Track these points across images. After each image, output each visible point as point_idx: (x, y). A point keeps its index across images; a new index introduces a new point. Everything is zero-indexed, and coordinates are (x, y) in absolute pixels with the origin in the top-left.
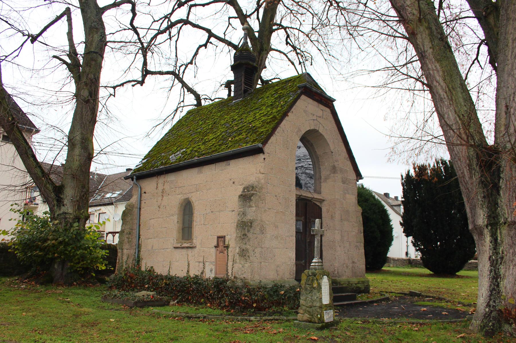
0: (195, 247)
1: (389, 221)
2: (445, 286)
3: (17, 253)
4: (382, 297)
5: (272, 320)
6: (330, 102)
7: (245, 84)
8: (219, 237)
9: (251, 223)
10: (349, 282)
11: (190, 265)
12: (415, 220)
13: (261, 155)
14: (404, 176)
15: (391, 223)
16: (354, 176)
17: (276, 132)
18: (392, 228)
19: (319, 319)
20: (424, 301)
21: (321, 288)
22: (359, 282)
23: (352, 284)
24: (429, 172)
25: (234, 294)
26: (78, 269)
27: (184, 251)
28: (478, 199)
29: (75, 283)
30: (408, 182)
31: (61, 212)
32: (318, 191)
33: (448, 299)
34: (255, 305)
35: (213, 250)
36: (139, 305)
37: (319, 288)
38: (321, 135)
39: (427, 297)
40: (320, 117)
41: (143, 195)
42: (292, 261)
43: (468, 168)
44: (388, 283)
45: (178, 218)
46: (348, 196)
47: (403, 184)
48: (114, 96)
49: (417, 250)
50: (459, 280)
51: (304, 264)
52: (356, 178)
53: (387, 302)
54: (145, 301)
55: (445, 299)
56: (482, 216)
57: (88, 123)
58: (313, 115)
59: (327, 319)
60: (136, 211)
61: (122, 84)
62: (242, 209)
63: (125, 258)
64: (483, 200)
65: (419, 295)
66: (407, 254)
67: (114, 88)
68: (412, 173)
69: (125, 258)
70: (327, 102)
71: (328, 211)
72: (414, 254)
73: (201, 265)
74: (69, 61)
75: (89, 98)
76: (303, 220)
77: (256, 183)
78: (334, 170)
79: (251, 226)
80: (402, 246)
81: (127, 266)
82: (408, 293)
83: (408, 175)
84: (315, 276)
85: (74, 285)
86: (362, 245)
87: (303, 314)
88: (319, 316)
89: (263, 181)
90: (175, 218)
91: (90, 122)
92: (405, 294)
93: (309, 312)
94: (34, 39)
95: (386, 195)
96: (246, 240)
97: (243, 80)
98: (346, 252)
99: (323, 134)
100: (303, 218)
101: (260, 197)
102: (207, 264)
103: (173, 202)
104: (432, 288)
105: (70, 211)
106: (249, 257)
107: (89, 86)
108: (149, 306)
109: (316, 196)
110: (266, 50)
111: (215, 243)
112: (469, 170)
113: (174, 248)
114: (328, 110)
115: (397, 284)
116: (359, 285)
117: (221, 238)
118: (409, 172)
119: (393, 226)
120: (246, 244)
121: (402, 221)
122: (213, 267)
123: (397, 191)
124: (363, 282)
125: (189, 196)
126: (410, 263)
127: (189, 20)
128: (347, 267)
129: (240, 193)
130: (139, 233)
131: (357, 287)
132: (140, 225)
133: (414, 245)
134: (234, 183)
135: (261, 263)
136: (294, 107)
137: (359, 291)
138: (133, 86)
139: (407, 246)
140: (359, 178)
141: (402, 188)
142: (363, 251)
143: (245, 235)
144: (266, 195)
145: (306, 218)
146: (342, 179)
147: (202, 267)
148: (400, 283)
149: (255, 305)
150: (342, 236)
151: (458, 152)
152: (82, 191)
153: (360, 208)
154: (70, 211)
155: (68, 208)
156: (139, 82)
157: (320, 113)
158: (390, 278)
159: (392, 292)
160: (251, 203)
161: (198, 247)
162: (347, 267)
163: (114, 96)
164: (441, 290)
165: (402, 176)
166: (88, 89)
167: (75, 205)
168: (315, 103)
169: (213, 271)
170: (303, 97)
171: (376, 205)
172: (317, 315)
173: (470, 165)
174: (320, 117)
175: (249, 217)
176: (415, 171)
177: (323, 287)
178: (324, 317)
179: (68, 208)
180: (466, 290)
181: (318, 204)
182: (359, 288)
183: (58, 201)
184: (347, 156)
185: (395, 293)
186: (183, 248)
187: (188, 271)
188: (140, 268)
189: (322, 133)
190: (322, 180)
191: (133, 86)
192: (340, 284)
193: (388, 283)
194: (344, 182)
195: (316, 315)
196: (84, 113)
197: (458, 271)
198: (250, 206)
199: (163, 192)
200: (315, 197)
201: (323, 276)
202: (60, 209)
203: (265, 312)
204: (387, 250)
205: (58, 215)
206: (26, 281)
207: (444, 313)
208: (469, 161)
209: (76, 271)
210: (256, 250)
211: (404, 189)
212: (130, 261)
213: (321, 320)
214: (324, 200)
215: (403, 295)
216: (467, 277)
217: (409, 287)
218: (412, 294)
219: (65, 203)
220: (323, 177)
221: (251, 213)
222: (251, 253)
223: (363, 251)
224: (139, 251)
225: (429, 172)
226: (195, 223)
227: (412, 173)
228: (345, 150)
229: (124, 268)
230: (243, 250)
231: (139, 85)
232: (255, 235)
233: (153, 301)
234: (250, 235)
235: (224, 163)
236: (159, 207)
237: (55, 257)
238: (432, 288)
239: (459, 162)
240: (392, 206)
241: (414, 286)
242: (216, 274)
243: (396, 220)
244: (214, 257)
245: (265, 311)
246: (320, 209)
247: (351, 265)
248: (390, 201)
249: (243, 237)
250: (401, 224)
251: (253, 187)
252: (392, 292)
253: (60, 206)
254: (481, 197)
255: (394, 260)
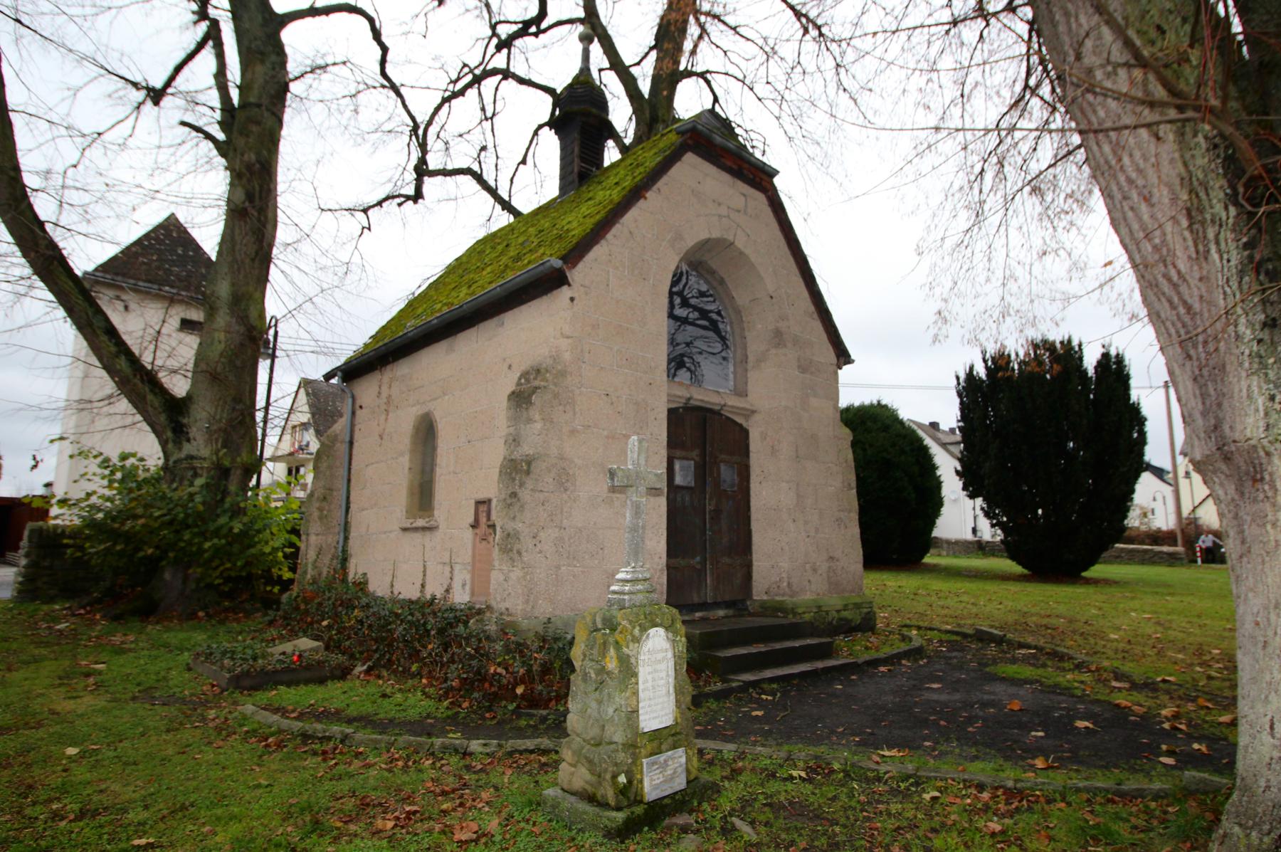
0: (436, 528)
1: (934, 468)
2: (1062, 609)
3: (67, 546)
4: (904, 647)
5: (532, 752)
6: (764, 177)
7: (582, 159)
8: (479, 503)
9: (529, 464)
10: (820, 607)
11: (428, 573)
12: (988, 464)
13: (565, 288)
14: (962, 376)
15: (938, 473)
16: (830, 355)
17: (609, 236)
18: (940, 483)
19: (623, 791)
20: (1014, 661)
21: (635, 675)
22: (846, 605)
23: (827, 612)
24: (1016, 367)
25: (472, 657)
26: (217, 582)
27: (417, 537)
28: (1238, 337)
29: (201, 614)
30: (974, 393)
31: (183, 455)
32: (741, 392)
33: (1081, 657)
34: (520, 690)
35: (469, 534)
36: (247, 682)
37: (628, 671)
38: (741, 253)
39: (1021, 646)
40: (739, 211)
41: (359, 412)
42: (657, 559)
43: (1185, 223)
44: (928, 599)
45: (411, 460)
46: (814, 402)
47: (960, 394)
48: (369, 229)
49: (993, 526)
50: (1091, 590)
51: (698, 567)
52: (834, 360)
53: (916, 660)
54: (267, 673)
55: (1071, 658)
56: (1261, 401)
57: (247, 261)
58: (720, 204)
59: (656, 787)
60: (342, 448)
61: (380, 203)
62: (512, 429)
63: (312, 555)
64: (1265, 335)
65: (999, 641)
66: (974, 531)
67: (365, 211)
68: (980, 371)
69: (312, 555)
70: (758, 177)
71: (764, 437)
72: (988, 532)
73: (448, 569)
74: (221, 136)
75: (247, 204)
76: (697, 459)
77: (549, 361)
78: (778, 338)
79: (528, 473)
80: (961, 516)
81: (315, 573)
82: (970, 631)
83: (970, 375)
84: (613, 629)
85: (197, 617)
86: (855, 516)
87: (574, 766)
88: (622, 779)
89: (567, 356)
90: (405, 461)
91: (253, 260)
92: (965, 636)
93: (590, 762)
94: (156, 96)
95: (934, 425)
96: (516, 508)
97: (577, 150)
98: (812, 534)
99: (748, 251)
100: (695, 453)
101: (556, 396)
102: (457, 568)
103: (404, 422)
104: (1032, 615)
105: (205, 452)
106: (519, 553)
107: (244, 180)
108: (277, 683)
109: (733, 401)
110: (664, 121)
111: (471, 519)
112: (1190, 227)
113: (405, 530)
114: (761, 197)
115: (949, 602)
116: (845, 614)
117: (482, 504)
118: (971, 368)
119: (942, 479)
120: (514, 518)
121: (959, 468)
122: (468, 577)
123: (948, 414)
124: (857, 606)
125: (430, 407)
126: (980, 547)
127: (512, 70)
128: (815, 570)
129: (511, 387)
130: (348, 498)
131: (841, 619)
132: (349, 481)
133: (987, 515)
134: (510, 367)
135: (558, 567)
136: (664, 179)
137: (848, 628)
138: (400, 205)
139: (975, 518)
140: (842, 360)
141: (957, 401)
142: (856, 530)
143: (514, 495)
144: (577, 392)
145: (703, 455)
146: (799, 360)
147: (448, 575)
148: (956, 599)
149: (520, 690)
150: (798, 496)
151: (1140, 171)
152: (234, 409)
153: (847, 431)
154: (205, 452)
155: (200, 446)
156: (408, 198)
157: (739, 202)
158: (937, 584)
159: (931, 629)
160: (531, 412)
161: (442, 526)
162: (815, 570)
163: (369, 229)
164: (1054, 621)
165: (958, 378)
166: (243, 187)
167: (217, 440)
168: (726, 177)
169: (468, 587)
170: (690, 158)
171: (905, 437)
172: (615, 777)
173: (1194, 214)
174: (739, 211)
175: (526, 449)
176: (987, 368)
177: (644, 672)
178: (641, 781)
179: (200, 446)
180: (1117, 622)
181: (739, 420)
182: (847, 621)
183: (174, 431)
184: (812, 308)
185: (939, 631)
186: (416, 529)
187: (423, 586)
188: (345, 574)
189: (743, 249)
190: (750, 365)
191: (400, 205)
192: (795, 614)
193: (928, 599)
194: (803, 369)
195: (608, 776)
196: (238, 238)
197: (1086, 569)
198: (530, 420)
199: (388, 403)
200: (730, 403)
201: (644, 629)
202: (180, 449)
203: (544, 712)
204: (931, 524)
205: (175, 462)
206: (82, 611)
207: (1081, 724)
208: (1191, 191)
209: (210, 586)
210: (542, 535)
211: (962, 403)
212: (326, 560)
213: (629, 794)
214: (753, 412)
215: (958, 638)
216: (1107, 582)
217: (974, 610)
218: (982, 637)
219: (191, 435)
220: (751, 358)
221: (534, 438)
222: (527, 542)
223: (857, 531)
224: (346, 539)
225: (1016, 367)
226: (438, 471)
227: (980, 371)
228: (806, 294)
229: (309, 576)
230: (509, 535)
231: (411, 202)
232: (542, 496)
233: (294, 670)
234: (525, 495)
235: (490, 324)
236: (381, 437)
237: (179, 555)
238: (1032, 615)
239: (1144, 207)
240: (944, 445)
241: (988, 609)
242: (472, 594)
243: (947, 466)
244: (470, 552)
245: (546, 707)
246: (745, 433)
247: (824, 567)
248: (940, 435)
249: (509, 501)
250: (957, 472)
251: (538, 371)
252: (931, 629)
253: (180, 443)
254: (1250, 324)
255: (948, 542)
